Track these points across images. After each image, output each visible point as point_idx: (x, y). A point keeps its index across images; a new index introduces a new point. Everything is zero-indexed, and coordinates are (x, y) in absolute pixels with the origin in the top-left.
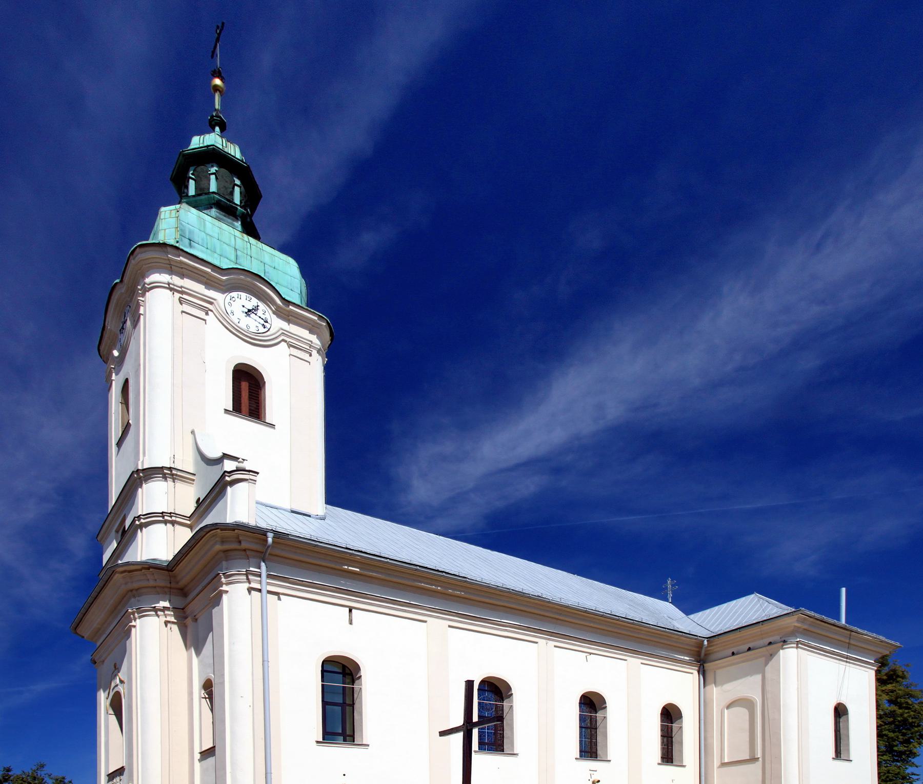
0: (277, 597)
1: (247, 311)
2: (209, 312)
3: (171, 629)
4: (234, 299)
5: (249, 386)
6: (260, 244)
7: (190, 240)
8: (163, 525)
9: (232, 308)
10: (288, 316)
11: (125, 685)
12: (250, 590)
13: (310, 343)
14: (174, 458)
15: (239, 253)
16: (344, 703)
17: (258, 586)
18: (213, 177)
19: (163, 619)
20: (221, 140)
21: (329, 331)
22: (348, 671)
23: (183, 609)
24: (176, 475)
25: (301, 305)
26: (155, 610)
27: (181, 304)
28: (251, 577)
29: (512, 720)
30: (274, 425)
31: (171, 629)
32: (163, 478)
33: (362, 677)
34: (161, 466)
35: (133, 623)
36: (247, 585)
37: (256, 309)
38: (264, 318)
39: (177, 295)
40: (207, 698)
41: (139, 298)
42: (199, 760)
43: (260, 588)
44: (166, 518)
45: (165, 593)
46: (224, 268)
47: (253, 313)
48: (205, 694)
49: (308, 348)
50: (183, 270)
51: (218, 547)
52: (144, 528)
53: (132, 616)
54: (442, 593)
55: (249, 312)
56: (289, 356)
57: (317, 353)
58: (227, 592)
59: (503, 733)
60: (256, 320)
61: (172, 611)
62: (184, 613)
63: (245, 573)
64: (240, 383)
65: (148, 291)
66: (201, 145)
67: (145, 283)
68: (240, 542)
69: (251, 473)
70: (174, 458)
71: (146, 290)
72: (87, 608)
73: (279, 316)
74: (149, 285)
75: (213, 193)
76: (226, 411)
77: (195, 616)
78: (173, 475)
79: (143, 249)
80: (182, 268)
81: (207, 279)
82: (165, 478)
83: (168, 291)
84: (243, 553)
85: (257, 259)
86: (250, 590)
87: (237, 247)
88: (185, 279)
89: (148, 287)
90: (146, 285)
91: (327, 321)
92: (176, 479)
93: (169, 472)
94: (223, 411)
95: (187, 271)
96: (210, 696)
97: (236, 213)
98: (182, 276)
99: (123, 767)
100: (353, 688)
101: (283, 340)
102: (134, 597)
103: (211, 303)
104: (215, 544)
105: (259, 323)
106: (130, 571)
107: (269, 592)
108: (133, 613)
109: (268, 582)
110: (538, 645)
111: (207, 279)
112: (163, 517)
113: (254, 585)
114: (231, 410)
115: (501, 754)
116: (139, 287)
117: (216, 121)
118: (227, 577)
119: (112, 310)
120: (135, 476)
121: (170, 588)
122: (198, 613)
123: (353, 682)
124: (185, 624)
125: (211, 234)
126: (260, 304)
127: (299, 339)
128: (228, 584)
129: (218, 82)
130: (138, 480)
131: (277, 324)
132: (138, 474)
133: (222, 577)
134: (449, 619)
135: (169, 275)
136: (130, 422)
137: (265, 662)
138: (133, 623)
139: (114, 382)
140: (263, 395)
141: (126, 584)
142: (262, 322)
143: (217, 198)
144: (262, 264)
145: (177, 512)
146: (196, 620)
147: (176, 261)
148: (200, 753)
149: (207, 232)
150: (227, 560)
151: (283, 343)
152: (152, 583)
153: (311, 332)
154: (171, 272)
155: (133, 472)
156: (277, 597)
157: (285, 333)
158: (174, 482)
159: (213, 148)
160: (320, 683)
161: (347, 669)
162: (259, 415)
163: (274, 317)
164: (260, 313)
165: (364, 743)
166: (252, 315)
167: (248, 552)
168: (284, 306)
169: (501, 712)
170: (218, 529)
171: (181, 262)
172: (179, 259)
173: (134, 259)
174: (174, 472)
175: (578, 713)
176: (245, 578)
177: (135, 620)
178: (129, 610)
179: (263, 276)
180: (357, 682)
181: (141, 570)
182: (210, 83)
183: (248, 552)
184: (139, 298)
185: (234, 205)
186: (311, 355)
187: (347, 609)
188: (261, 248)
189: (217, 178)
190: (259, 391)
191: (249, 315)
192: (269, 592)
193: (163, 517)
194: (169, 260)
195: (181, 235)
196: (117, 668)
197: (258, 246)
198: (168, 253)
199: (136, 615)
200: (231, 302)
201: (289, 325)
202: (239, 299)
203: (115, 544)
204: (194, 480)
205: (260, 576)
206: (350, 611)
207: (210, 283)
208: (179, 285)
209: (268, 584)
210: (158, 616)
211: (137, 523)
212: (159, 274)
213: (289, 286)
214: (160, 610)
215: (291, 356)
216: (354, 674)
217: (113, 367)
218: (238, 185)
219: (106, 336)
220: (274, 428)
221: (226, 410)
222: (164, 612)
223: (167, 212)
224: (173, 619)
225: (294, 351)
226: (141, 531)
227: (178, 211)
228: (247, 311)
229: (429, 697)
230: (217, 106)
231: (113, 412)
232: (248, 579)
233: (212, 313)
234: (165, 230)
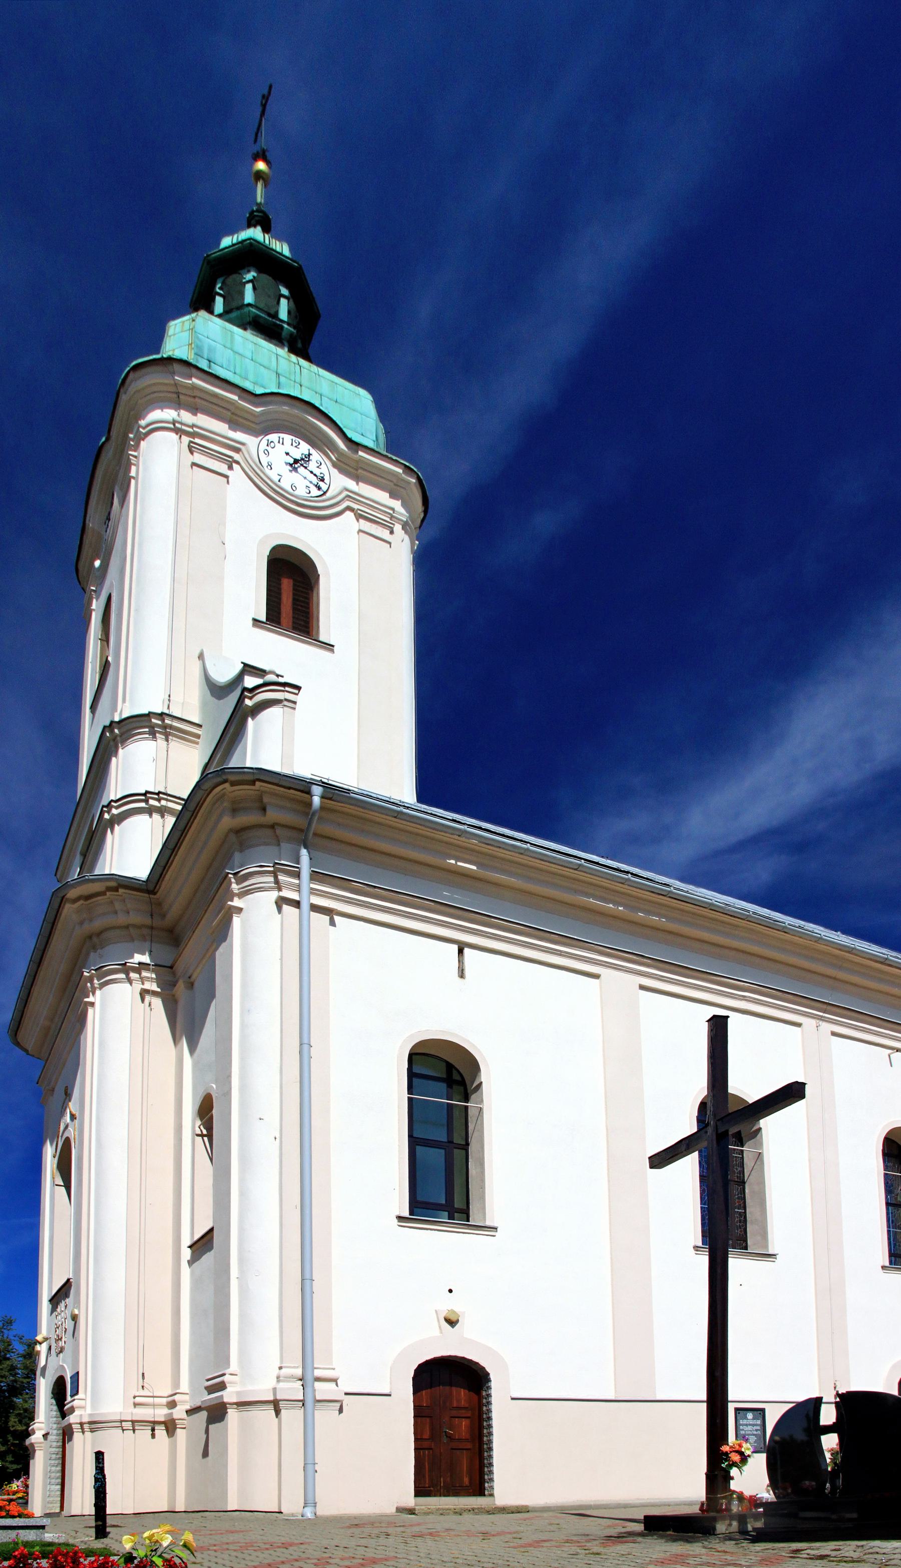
0: (328, 918)
1: (292, 461)
2: (234, 465)
3: (150, 1005)
4: (272, 445)
5: (294, 585)
6: (314, 368)
7: (210, 361)
8: (145, 817)
9: (270, 459)
10: (357, 470)
11: (76, 1121)
12: (281, 902)
13: (391, 512)
14: (169, 700)
15: (282, 379)
16: (450, 1142)
17: (294, 896)
18: (249, 287)
19: (138, 986)
20: (262, 235)
21: (421, 494)
22: (456, 1077)
23: (171, 967)
24: (171, 727)
25: (375, 448)
26: (126, 969)
27: (192, 453)
28: (282, 878)
29: (762, 1182)
30: (333, 646)
31: (150, 1005)
32: (149, 734)
33: (484, 1085)
34: (147, 712)
35: (91, 999)
36: (274, 895)
37: (307, 458)
38: (318, 474)
39: (186, 440)
40: (205, 1136)
41: (130, 452)
42: (188, 1261)
43: (297, 898)
44: (152, 802)
45: (143, 938)
47: (302, 465)
48: (202, 1127)
49: (388, 520)
50: (197, 400)
51: (227, 822)
52: (116, 825)
53: (89, 984)
54: (624, 920)
55: (295, 464)
56: (358, 533)
57: (403, 529)
58: (239, 910)
59: (745, 1212)
60: (305, 478)
61: (153, 971)
62: (174, 974)
63: (272, 869)
64: (280, 580)
67: (140, 426)
68: (264, 809)
69: (287, 689)
70: (169, 700)
71: (141, 437)
72: (29, 987)
73: (342, 471)
75: (249, 305)
76: (256, 622)
77: (189, 977)
78: (165, 727)
79: (138, 373)
80: (194, 397)
81: (233, 413)
82: (153, 734)
84: (269, 832)
85: (309, 388)
86: (281, 902)
87: (280, 371)
88: (199, 414)
89: (144, 431)
91: (418, 475)
93: (160, 722)
94: (251, 622)
96: (208, 1125)
97: (280, 334)
98: (194, 410)
99: (68, 1280)
100: (466, 1108)
101: (349, 508)
102: (94, 948)
103: (238, 450)
104: (220, 817)
105: (311, 482)
106: (88, 897)
107: (315, 908)
108: (91, 980)
109: (312, 889)
110: (802, 1031)
111: (233, 413)
112: (146, 801)
113: (286, 893)
114: (264, 619)
115: (742, 1254)
116: (131, 436)
118: (241, 879)
119: (95, 502)
120: (108, 734)
121: (152, 928)
122: (194, 971)
123: (467, 1099)
124: (174, 996)
125: (241, 351)
126: (313, 451)
127: (373, 504)
128: (242, 894)
129: (261, 166)
130: (112, 743)
131: (339, 482)
132: (112, 732)
133: (233, 880)
134: (636, 970)
135: (176, 410)
136: (110, 659)
137: (304, 1045)
138: (91, 999)
139: (94, 614)
140: (315, 599)
141: (81, 923)
142: (315, 480)
143: (255, 313)
144: (318, 396)
145: (169, 792)
146: (192, 984)
147: (186, 387)
148: (190, 1247)
149: (235, 350)
150: (241, 851)
151: (348, 513)
152: (122, 919)
153: (393, 496)
154: (178, 404)
155: (105, 727)
156: (328, 918)
157: (351, 496)
158: (167, 740)
160: (406, 1095)
161: (454, 1072)
162: (308, 627)
163: (334, 472)
164: (312, 466)
165: (488, 1223)
166: (301, 470)
167: (279, 831)
168: (350, 452)
169: (739, 1169)
170: (225, 781)
171: (194, 387)
172: (190, 382)
173: (125, 393)
174: (167, 721)
175: (882, 1172)
176: (272, 879)
177: (94, 994)
178: (85, 974)
179: (317, 405)
180: (473, 1097)
182: (252, 165)
183: (279, 831)
184: (130, 452)
185: (278, 322)
186: (392, 532)
187: (455, 948)
188: (317, 372)
189: (254, 288)
190: (310, 592)
191: (295, 470)
192: (315, 908)
193: (146, 801)
194: (176, 384)
195: (196, 354)
196: (68, 1095)
197: (312, 370)
198: (173, 373)
199: (96, 981)
200: (269, 449)
201: (357, 484)
202: (280, 445)
203: (79, 869)
204: (198, 736)
205: (298, 875)
206: (461, 951)
207: (236, 420)
208: (190, 422)
209: (313, 892)
210: (130, 981)
211: (106, 816)
212: (160, 411)
213: (359, 429)
214: (135, 970)
215: (360, 533)
216: (468, 1082)
217: (94, 588)
218: (285, 297)
219: (86, 542)
220: (333, 651)
221: (255, 620)
222: (140, 974)
223: (178, 325)
224: (154, 987)
225: (365, 525)
226: (112, 832)
227: (193, 320)
228: (292, 461)
229: (607, 1129)
230: (259, 200)
231: (90, 660)
232: (277, 881)
233: (238, 466)
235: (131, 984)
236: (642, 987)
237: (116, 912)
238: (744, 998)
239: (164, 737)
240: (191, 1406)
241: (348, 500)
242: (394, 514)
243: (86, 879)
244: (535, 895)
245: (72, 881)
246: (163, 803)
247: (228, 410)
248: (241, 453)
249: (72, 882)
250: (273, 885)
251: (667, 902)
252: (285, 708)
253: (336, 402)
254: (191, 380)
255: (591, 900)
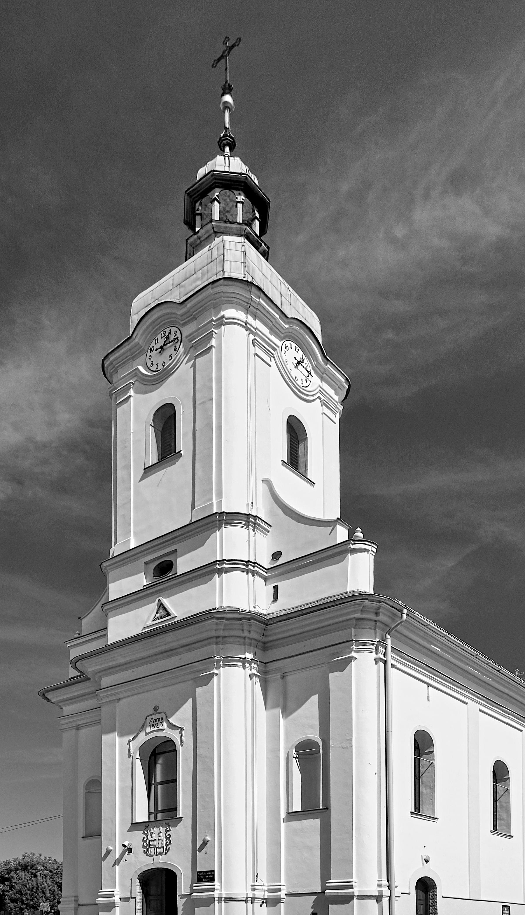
19: (249, 672)
23: (265, 663)
24: (259, 525)
30: (314, 483)
36: (374, 656)
39: (252, 337)
40: (297, 758)
46: (289, 317)
50: (258, 311)
65: (224, 325)
66: (227, 169)
69: (373, 545)
74: (226, 319)
78: (255, 524)
79: (227, 282)
80: (257, 309)
81: (273, 325)
83: (244, 330)
88: (257, 320)
90: (224, 319)
92: (257, 528)
93: (253, 520)
95: (260, 313)
98: (255, 317)
102: (217, 643)
103: (275, 350)
110: (523, 734)
112: (247, 566)
117: (229, 141)
133: (354, 644)
154: (247, 311)
159: (247, 177)
160: (413, 756)
171: (259, 304)
172: (258, 300)
173: (212, 288)
174: (258, 521)
176: (374, 648)
181: (241, 619)
193: (247, 566)
200: (286, 350)
201: (321, 382)
204: (268, 532)
206: (428, 687)
210: (244, 667)
215: (324, 415)
220: (313, 486)
230: (227, 125)
231: (132, 431)
234: (231, 261)
235: (244, 669)
236: (480, 710)
237: (243, 630)
238: (508, 718)
239: (252, 528)
240: (24, 856)
241: (319, 393)
242: (337, 406)
243: (238, 613)
244: (452, 663)
245: (228, 611)
246: (256, 569)
247: (272, 322)
248: (276, 351)
249: (227, 612)
250: (375, 651)
251: (495, 672)
252: (370, 555)
253: (305, 319)
254: (259, 299)
255: (471, 668)
